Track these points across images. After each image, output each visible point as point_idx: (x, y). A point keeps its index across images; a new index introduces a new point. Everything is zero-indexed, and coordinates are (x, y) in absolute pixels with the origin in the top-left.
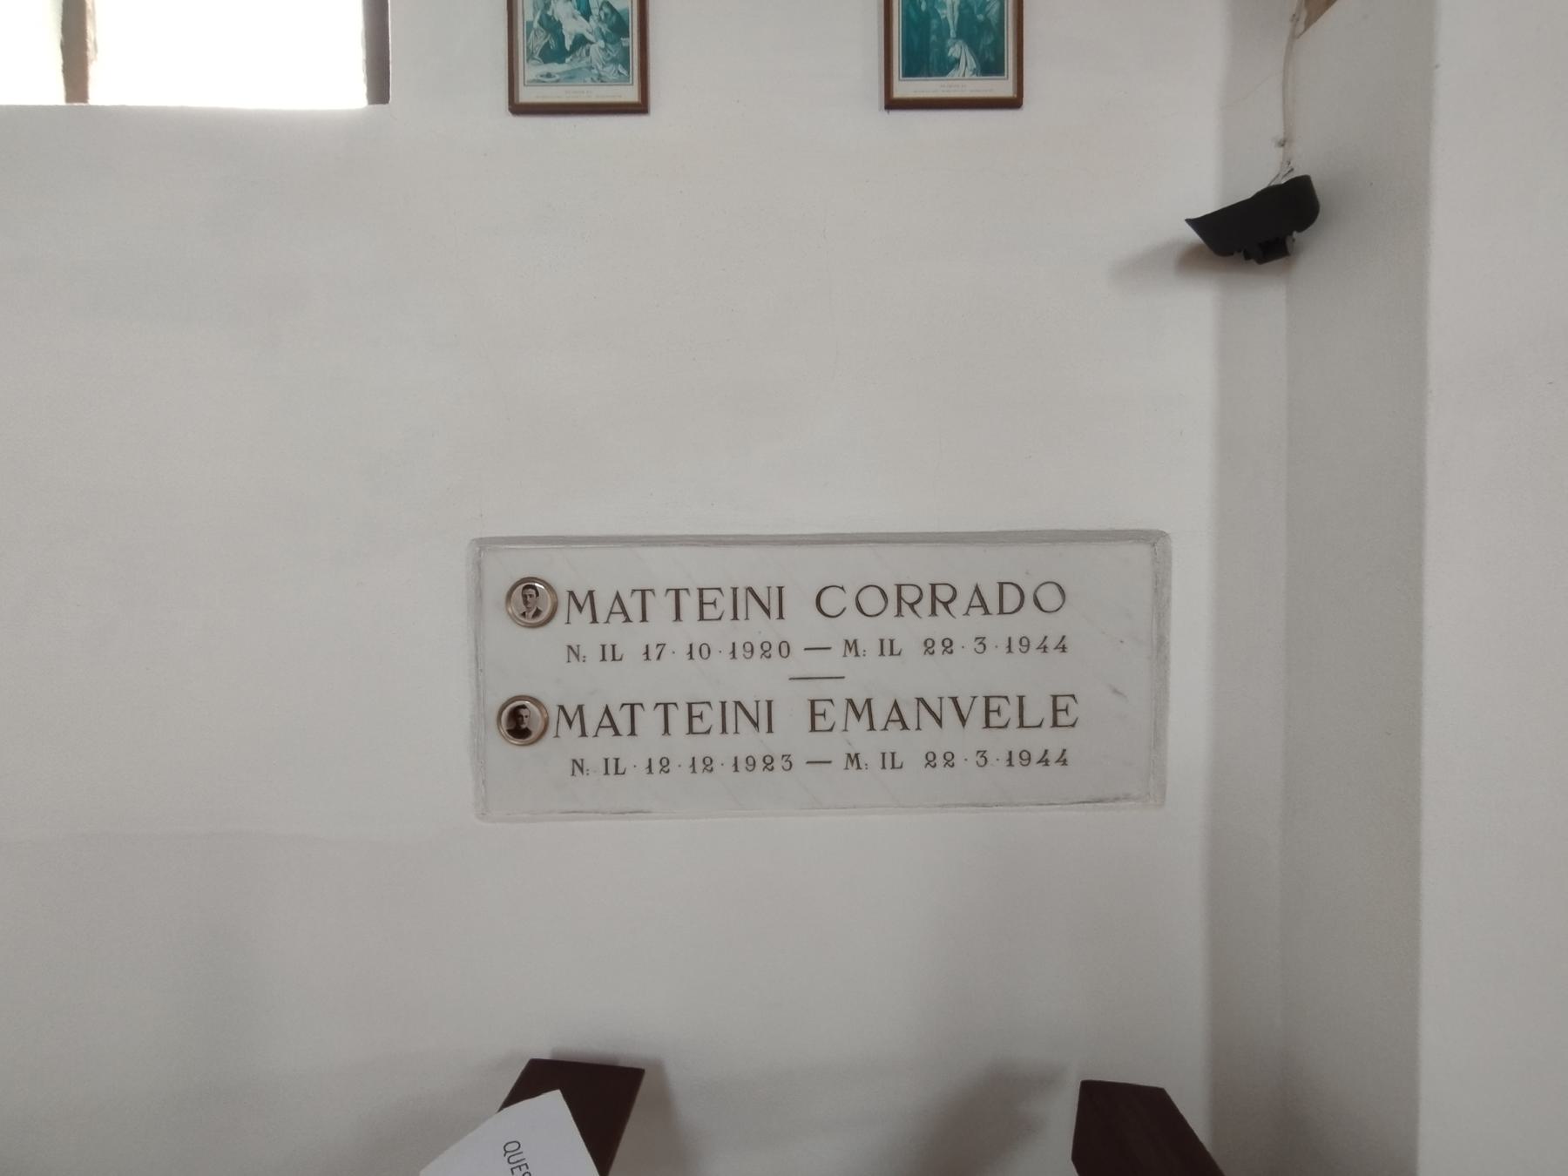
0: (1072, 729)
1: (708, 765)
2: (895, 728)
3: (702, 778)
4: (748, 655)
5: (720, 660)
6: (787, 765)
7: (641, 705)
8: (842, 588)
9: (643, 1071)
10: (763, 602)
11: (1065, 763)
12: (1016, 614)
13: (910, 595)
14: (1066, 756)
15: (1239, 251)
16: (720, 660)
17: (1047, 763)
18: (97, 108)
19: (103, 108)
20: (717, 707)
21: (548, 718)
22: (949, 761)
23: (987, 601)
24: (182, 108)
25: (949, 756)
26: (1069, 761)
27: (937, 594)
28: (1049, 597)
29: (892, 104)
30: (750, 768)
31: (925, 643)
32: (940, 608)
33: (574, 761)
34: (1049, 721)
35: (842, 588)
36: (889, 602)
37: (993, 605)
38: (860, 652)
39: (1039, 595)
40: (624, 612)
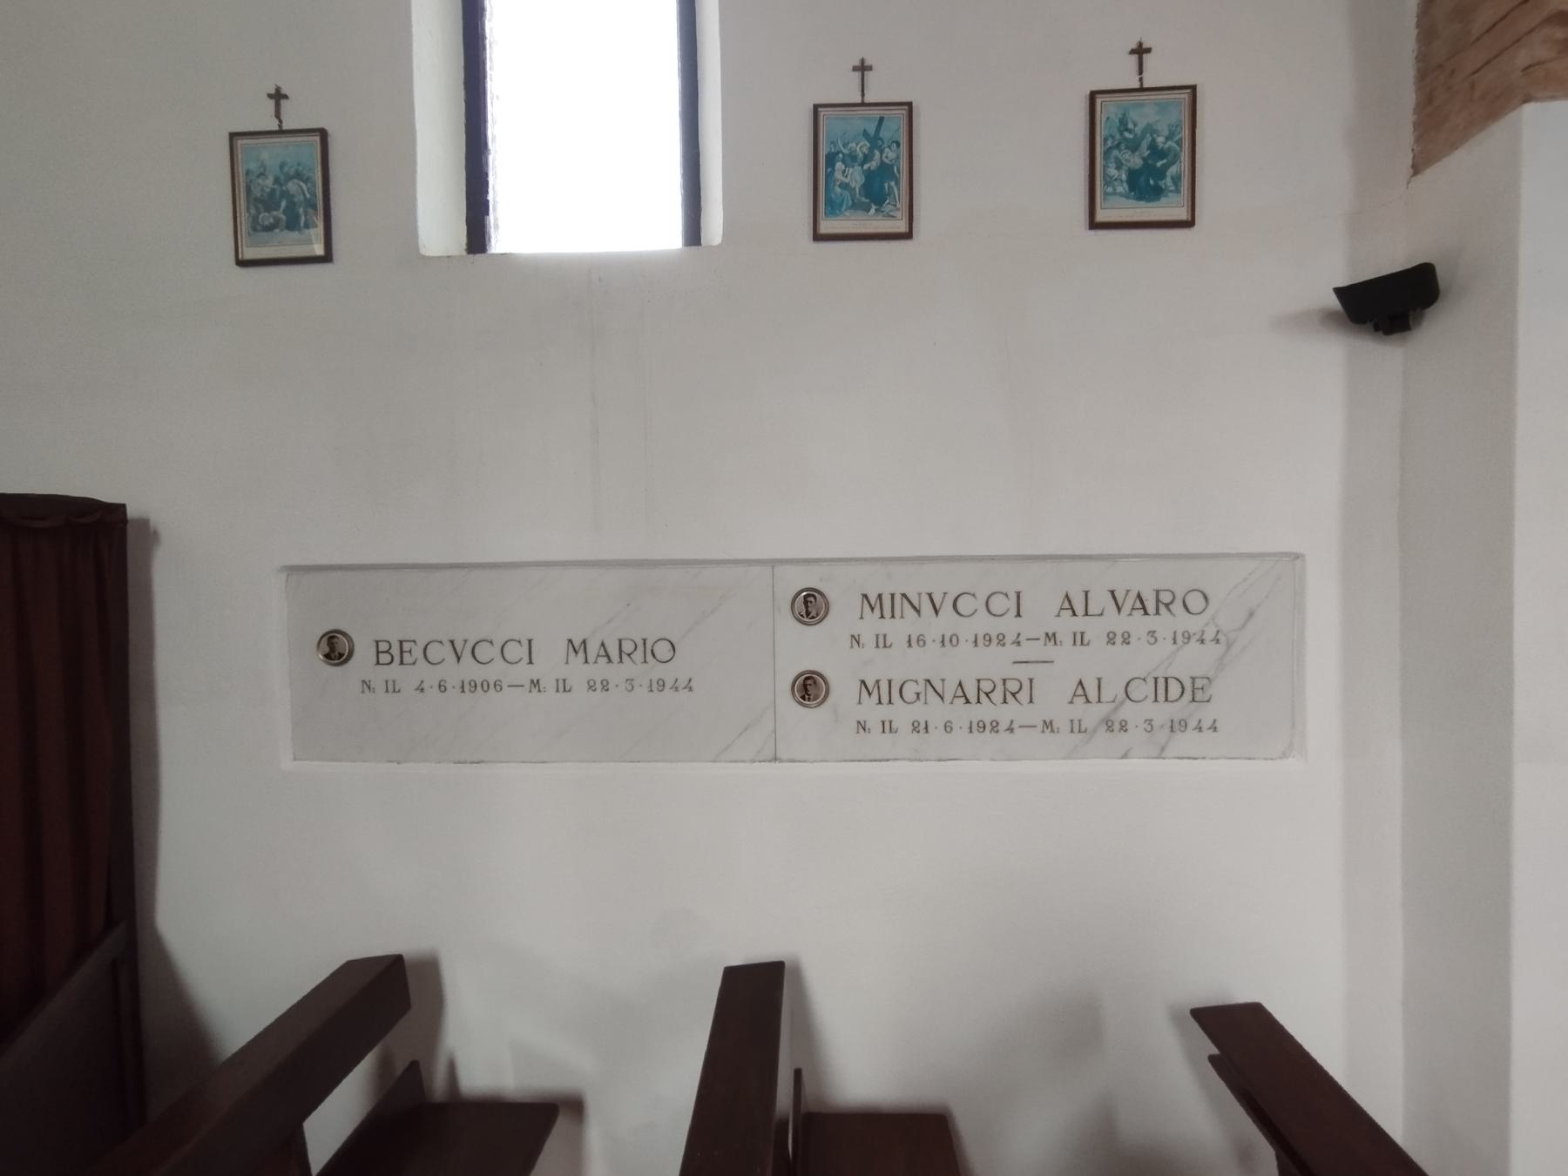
2: (1080, 701)
4: (987, 643)
5: (966, 647)
8: (974, 595)
10: (1118, 600)
11: (1215, 729)
15: (1371, 321)
16: (966, 647)
17: (1200, 729)
22: (605, 688)
25: (1123, 724)
26: (694, 688)
30: (982, 730)
32: (1162, 609)
33: (859, 722)
35: (974, 595)
37: (1079, 609)
39: (1204, 604)
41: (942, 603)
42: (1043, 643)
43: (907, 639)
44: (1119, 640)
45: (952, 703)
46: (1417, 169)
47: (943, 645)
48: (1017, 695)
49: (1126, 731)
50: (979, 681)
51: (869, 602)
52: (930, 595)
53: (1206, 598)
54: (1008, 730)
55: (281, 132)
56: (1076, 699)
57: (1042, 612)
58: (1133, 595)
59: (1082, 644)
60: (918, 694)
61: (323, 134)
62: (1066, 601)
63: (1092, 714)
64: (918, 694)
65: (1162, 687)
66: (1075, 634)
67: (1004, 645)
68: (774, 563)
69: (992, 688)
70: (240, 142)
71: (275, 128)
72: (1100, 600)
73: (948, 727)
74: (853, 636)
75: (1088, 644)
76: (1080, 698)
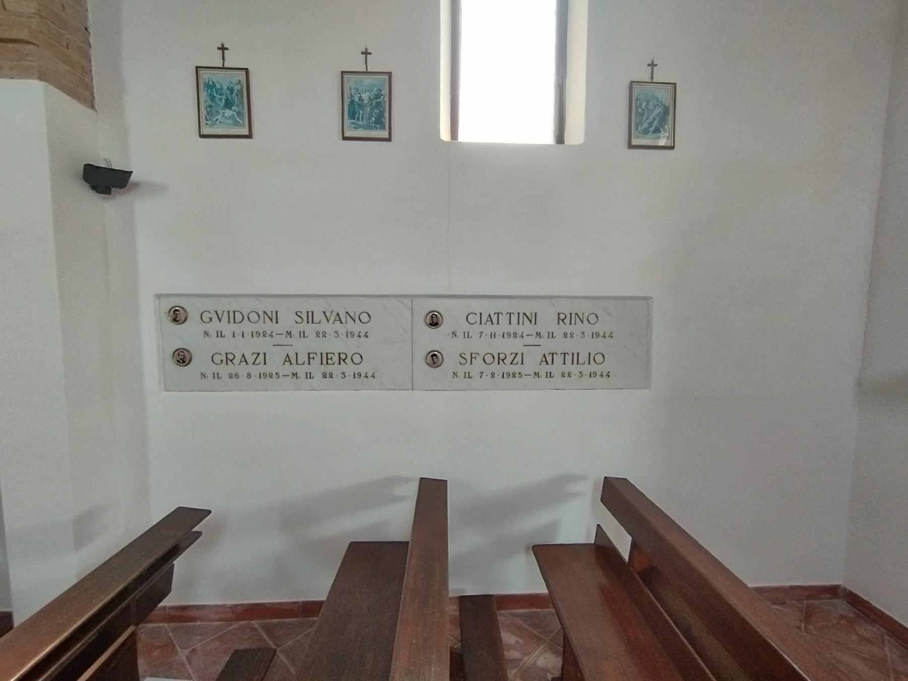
0: (303, 366)
1: (237, 376)
3: (592, 379)
4: (258, 336)
6: (344, 376)
7: (556, 353)
9: (444, 483)
12: (256, 324)
13: (562, 317)
14: (609, 374)
16: (248, 337)
18: (587, 135)
19: (463, 142)
20: (319, 355)
21: (192, 357)
23: (341, 318)
24: (501, 143)
26: (610, 376)
27: (560, 317)
28: (365, 318)
29: (631, 146)
31: (564, 334)
34: (307, 362)
36: (261, 318)
38: (292, 336)
40: (492, 321)
41: (330, 317)
42: (285, 336)
43: (232, 334)
44: (321, 335)
45: (240, 364)
46: (92, 107)
47: (504, 337)
48: (233, 361)
49: (332, 377)
50: (499, 354)
51: (268, 315)
52: (216, 312)
53: (369, 316)
54: (372, 376)
55: (223, 68)
56: (542, 363)
57: (287, 320)
58: (335, 314)
59: (221, 337)
60: (222, 361)
61: (632, 83)
62: (489, 318)
63: (224, 370)
64: (222, 361)
65: (326, 358)
66: (300, 332)
67: (266, 336)
68: (412, 297)
69: (504, 357)
70: (346, 76)
71: (364, 70)
72: (318, 316)
73: (249, 376)
74: (205, 332)
75: (224, 337)
76: (288, 362)
